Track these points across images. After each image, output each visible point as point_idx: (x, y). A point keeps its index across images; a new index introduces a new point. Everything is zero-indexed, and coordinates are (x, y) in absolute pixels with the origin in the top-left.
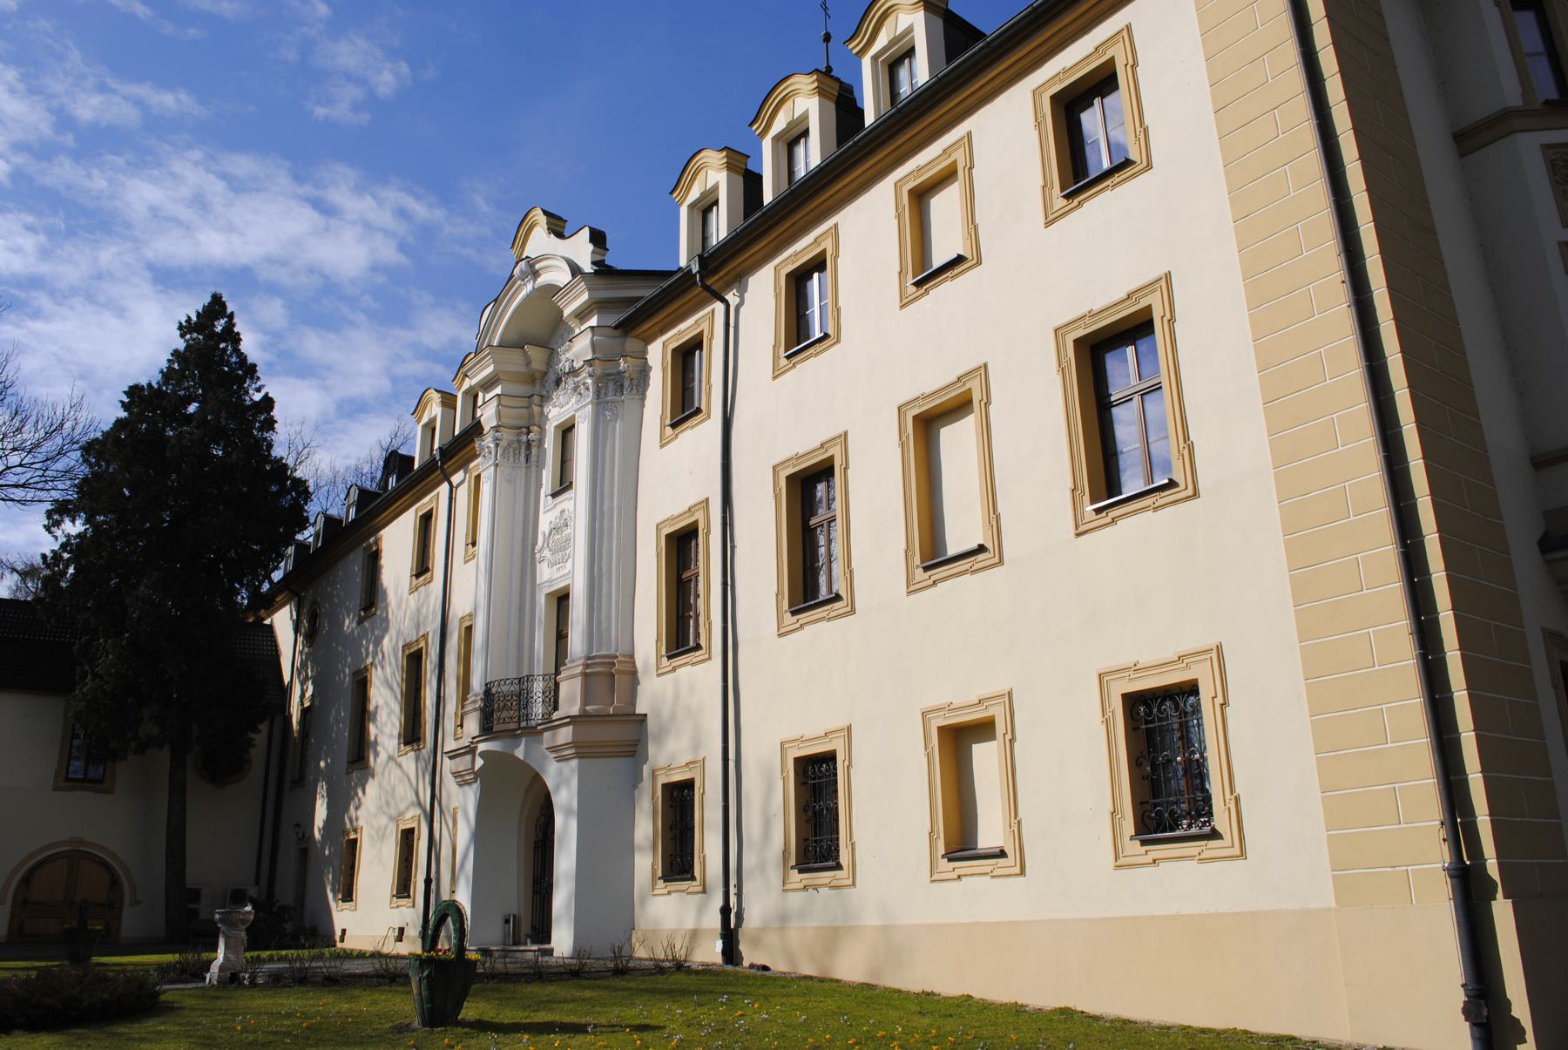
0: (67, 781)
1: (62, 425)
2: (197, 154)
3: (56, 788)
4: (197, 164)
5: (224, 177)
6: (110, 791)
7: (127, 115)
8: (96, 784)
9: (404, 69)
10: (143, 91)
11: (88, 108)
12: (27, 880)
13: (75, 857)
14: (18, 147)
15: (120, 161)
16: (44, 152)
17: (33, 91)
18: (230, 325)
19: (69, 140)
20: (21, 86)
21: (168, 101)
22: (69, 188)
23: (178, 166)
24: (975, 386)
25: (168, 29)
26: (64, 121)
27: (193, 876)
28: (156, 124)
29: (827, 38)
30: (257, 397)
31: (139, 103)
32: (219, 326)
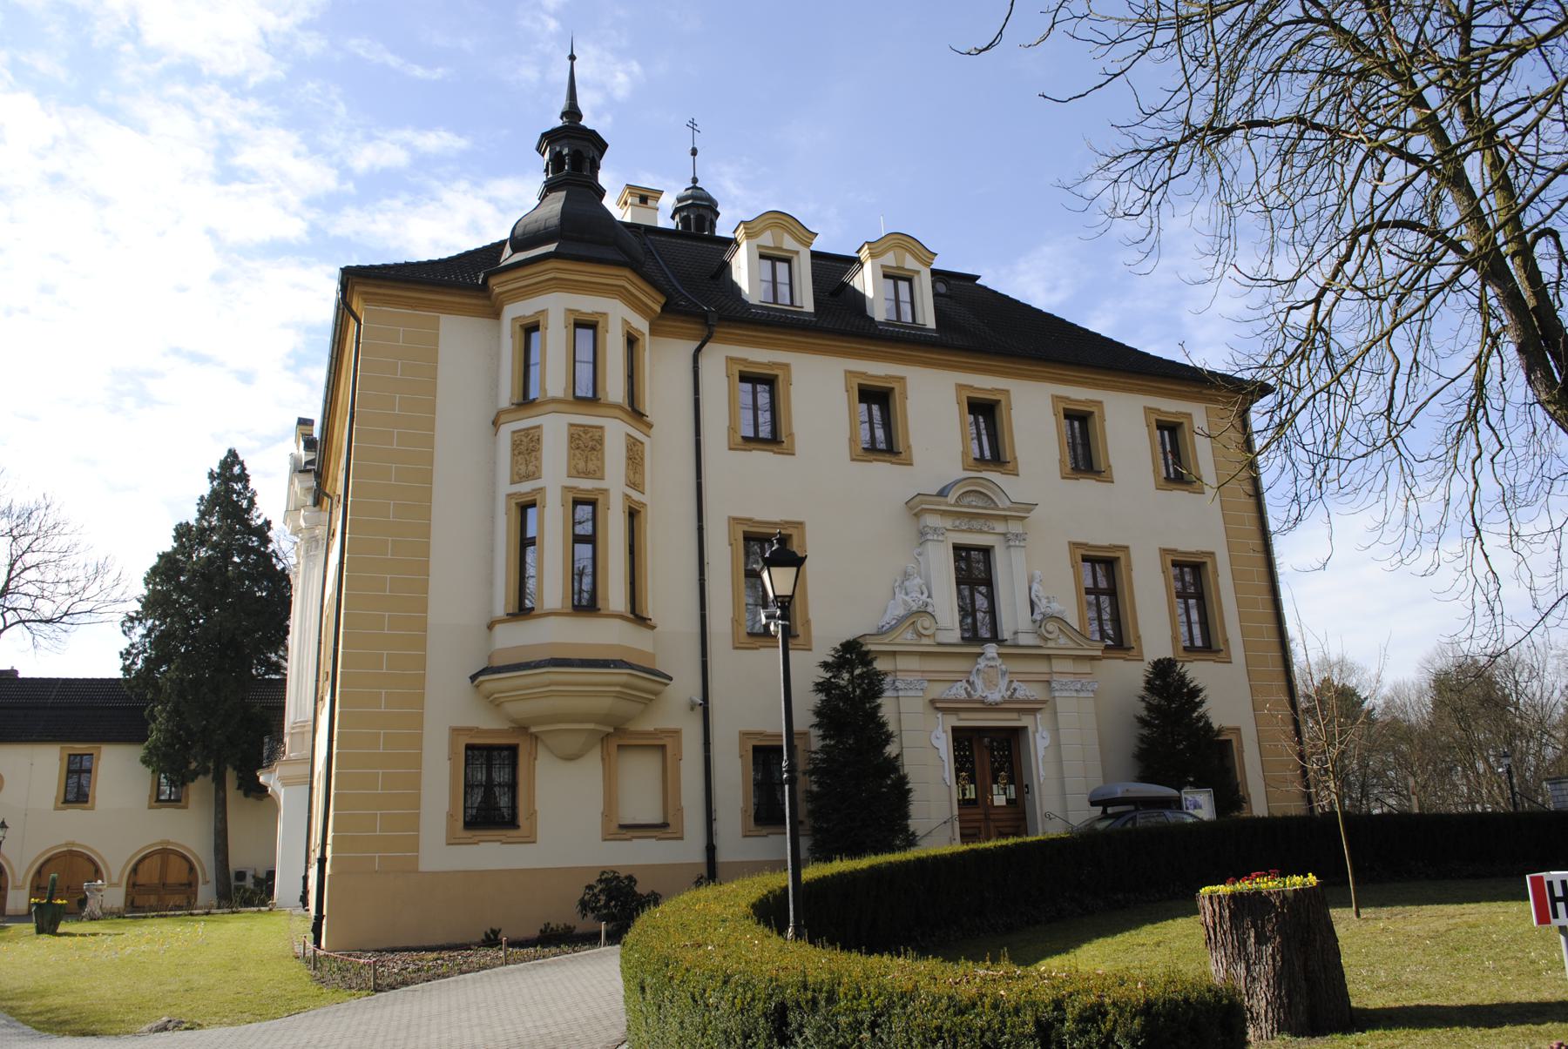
0: (158, 801)
1: (1205, 171)
2: (463, 185)
3: (150, 807)
4: (465, 192)
5: (490, 200)
6: (185, 807)
7: (395, 157)
8: (176, 802)
9: (636, 67)
10: (407, 134)
11: (366, 158)
12: (135, 870)
13: (165, 854)
14: (312, 203)
15: (397, 204)
16: (331, 203)
17: (315, 150)
18: (243, 469)
19: (350, 186)
20: (303, 148)
21: (434, 141)
22: (358, 234)
23: (448, 196)
24: (538, 497)
25: (419, 72)
26: (346, 173)
27: (234, 865)
28: (423, 162)
29: (694, 152)
30: (260, 522)
31: (407, 146)
32: (237, 470)
